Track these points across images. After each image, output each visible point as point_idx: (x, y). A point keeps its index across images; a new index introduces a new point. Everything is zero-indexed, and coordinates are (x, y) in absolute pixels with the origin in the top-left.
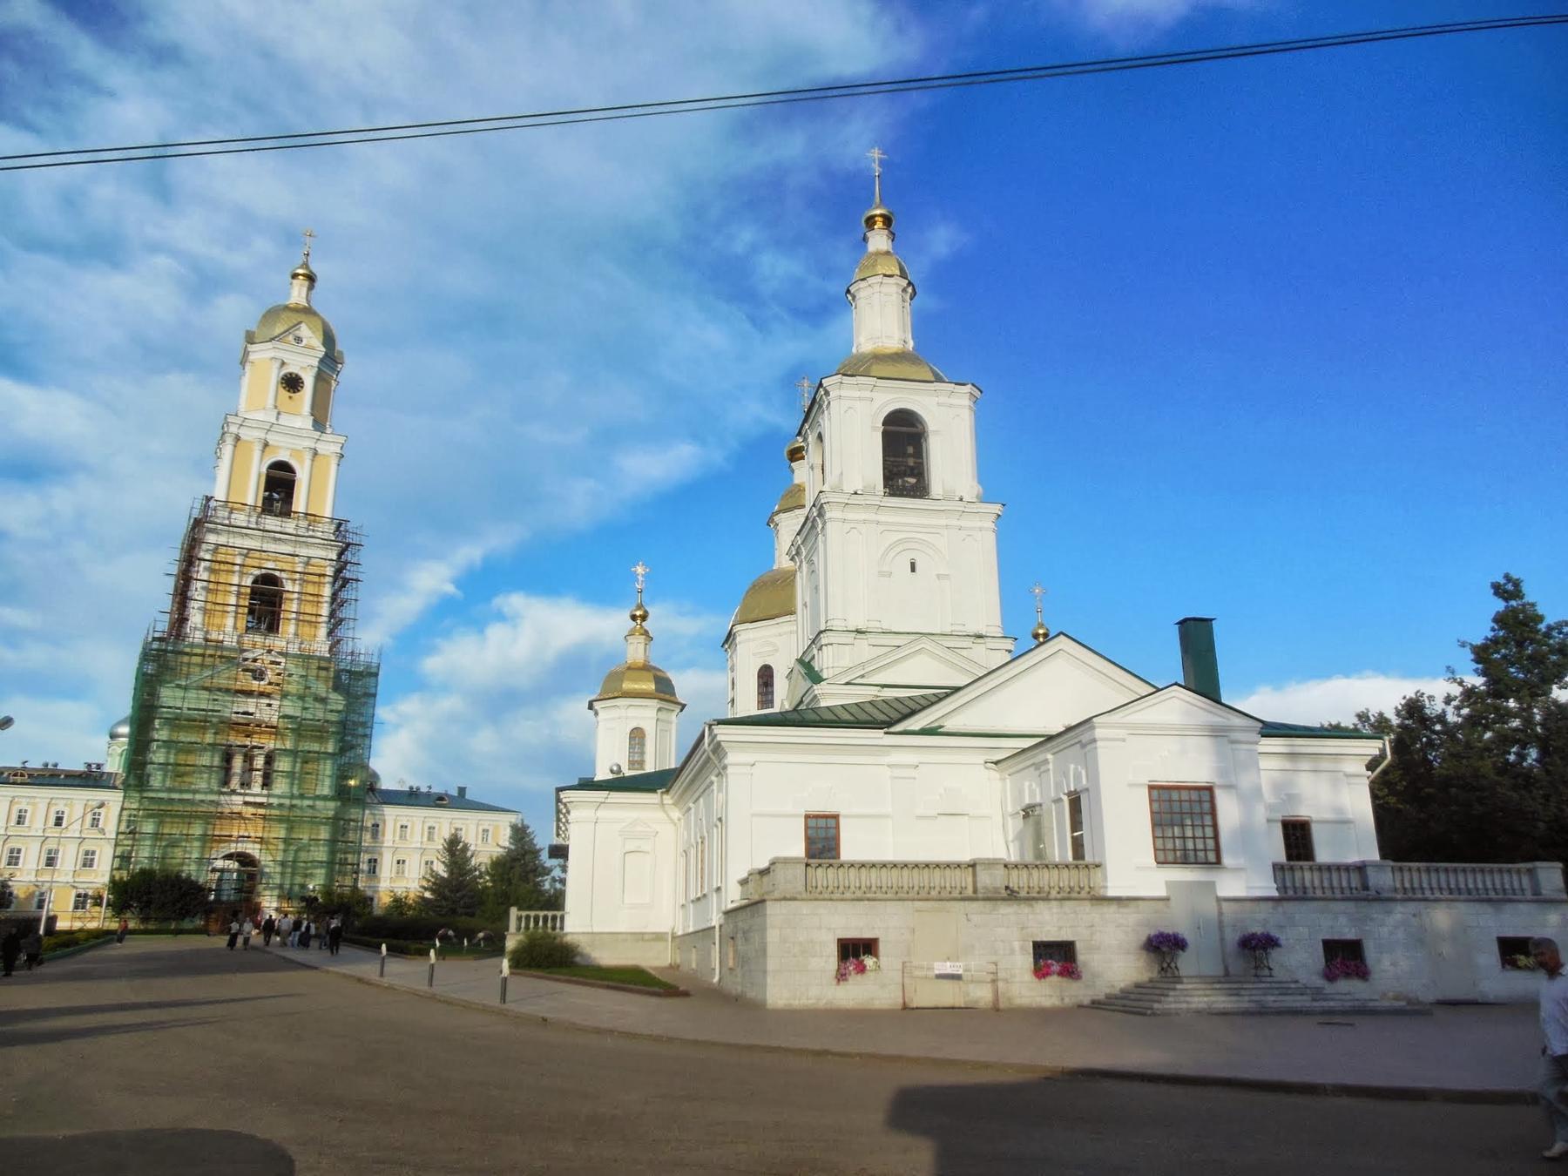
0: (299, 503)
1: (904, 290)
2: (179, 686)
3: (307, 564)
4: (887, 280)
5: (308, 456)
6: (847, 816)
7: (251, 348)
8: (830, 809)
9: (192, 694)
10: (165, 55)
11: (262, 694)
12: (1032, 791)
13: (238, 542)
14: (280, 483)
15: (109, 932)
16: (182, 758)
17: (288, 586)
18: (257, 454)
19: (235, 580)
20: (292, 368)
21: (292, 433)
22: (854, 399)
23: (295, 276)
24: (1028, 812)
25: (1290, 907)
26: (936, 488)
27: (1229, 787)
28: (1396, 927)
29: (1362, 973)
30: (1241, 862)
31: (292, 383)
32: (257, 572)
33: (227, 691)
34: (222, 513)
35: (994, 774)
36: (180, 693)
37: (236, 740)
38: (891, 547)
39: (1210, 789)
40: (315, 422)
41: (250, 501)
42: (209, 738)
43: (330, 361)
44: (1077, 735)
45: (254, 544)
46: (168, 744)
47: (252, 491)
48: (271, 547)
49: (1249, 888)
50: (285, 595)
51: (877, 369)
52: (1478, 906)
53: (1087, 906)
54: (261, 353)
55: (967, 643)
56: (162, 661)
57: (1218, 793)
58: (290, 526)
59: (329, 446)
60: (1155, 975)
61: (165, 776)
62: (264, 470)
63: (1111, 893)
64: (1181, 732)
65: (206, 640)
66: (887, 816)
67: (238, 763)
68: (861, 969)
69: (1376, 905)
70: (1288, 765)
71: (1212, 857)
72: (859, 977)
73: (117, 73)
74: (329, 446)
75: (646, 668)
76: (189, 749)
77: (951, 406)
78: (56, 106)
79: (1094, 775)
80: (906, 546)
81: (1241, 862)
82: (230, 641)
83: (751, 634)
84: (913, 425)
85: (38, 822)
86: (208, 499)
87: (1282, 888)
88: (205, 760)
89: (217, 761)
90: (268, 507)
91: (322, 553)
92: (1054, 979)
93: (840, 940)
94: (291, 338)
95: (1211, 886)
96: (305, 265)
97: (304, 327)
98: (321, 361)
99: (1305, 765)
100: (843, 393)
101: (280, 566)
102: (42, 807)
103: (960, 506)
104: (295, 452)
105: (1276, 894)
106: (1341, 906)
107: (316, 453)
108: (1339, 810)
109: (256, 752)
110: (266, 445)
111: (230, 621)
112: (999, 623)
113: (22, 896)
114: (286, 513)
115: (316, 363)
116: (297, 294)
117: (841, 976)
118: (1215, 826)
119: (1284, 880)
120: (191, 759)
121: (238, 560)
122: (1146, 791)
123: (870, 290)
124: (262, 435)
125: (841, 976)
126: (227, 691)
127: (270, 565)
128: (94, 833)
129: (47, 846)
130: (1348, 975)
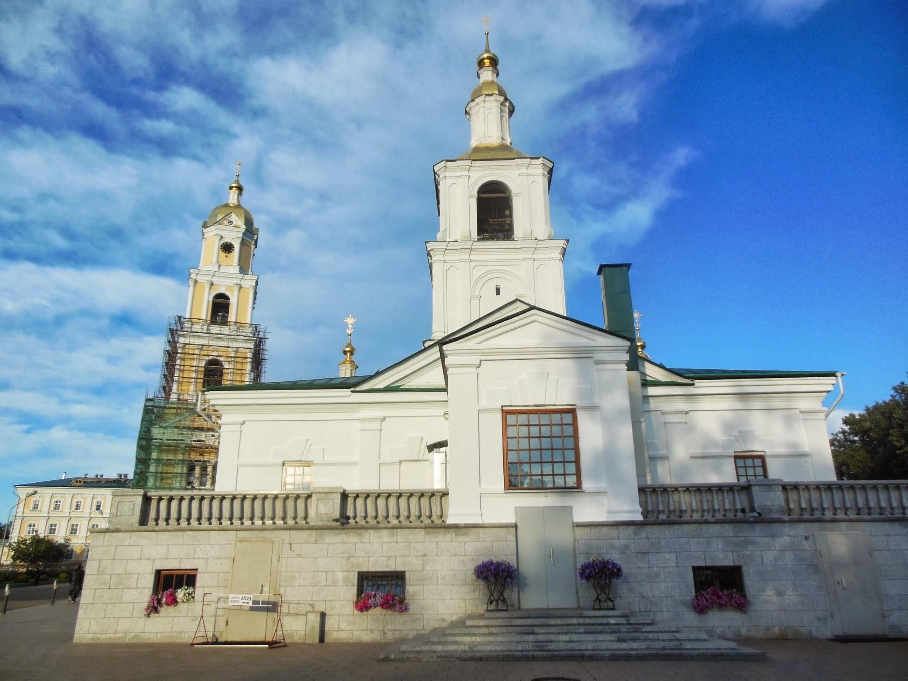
0: (232, 317)
1: (502, 104)
2: (161, 427)
3: (236, 352)
4: (488, 98)
7: (205, 230)
9: (169, 431)
10: (258, 113)
11: (209, 430)
13: (197, 341)
14: (220, 306)
16: (166, 469)
17: (226, 365)
18: (207, 289)
19: (195, 363)
20: (227, 239)
21: (226, 276)
23: (231, 188)
25: (655, 532)
27: (592, 408)
28: (783, 551)
29: (741, 604)
30: (603, 485)
33: (189, 428)
34: (187, 325)
36: (162, 430)
37: (194, 456)
39: (572, 411)
40: (241, 269)
41: (204, 317)
42: (180, 456)
43: (250, 231)
45: (205, 341)
46: (158, 461)
47: (204, 311)
48: (216, 343)
49: (610, 512)
50: (225, 371)
52: (887, 526)
53: (420, 535)
54: (211, 232)
56: (153, 414)
57: (580, 414)
58: (225, 330)
59: (248, 282)
60: (481, 609)
61: (156, 480)
62: (211, 299)
63: (450, 521)
64: (538, 354)
65: (179, 399)
66: (355, 463)
67: (197, 470)
68: (173, 601)
69: (758, 528)
70: (737, 405)
71: (571, 481)
72: (171, 609)
73: (237, 126)
74: (248, 282)
76: (169, 463)
78: (209, 145)
80: (490, 277)
81: (603, 485)
82: (191, 399)
84: (504, 192)
86: (180, 318)
87: (645, 513)
88: (178, 469)
89: (185, 470)
90: (214, 321)
91: (244, 345)
92: (378, 611)
93: (158, 572)
94: (226, 222)
95: (567, 510)
96: (237, 181)
97: (233, 215)
98: (244, 234)
99: (757, 404)
100: (448, 174)
101: (222, 354)
104: (228, 287)
105: (640, 517)
106: (714, 529)
107: (240, 287)
108: (794, 445)
109: (208, 464)
110: (212, 284)
111: (192, 388)
113: (78, 552)
114: (225, 323)
115: (240, 235)
116: (232, 198)
117: (153, 609)
118: (576, 450)
119: (646, 502)
120: (170, 469)
121: (197, 352)
122: (733, 459)
123: (477, 108)
124: (209, 279)
125: (153, 609)
126: (189, 428)
127: (215, 353)
128: (98, 514)
129: (50, 522)
130: (722, 607)
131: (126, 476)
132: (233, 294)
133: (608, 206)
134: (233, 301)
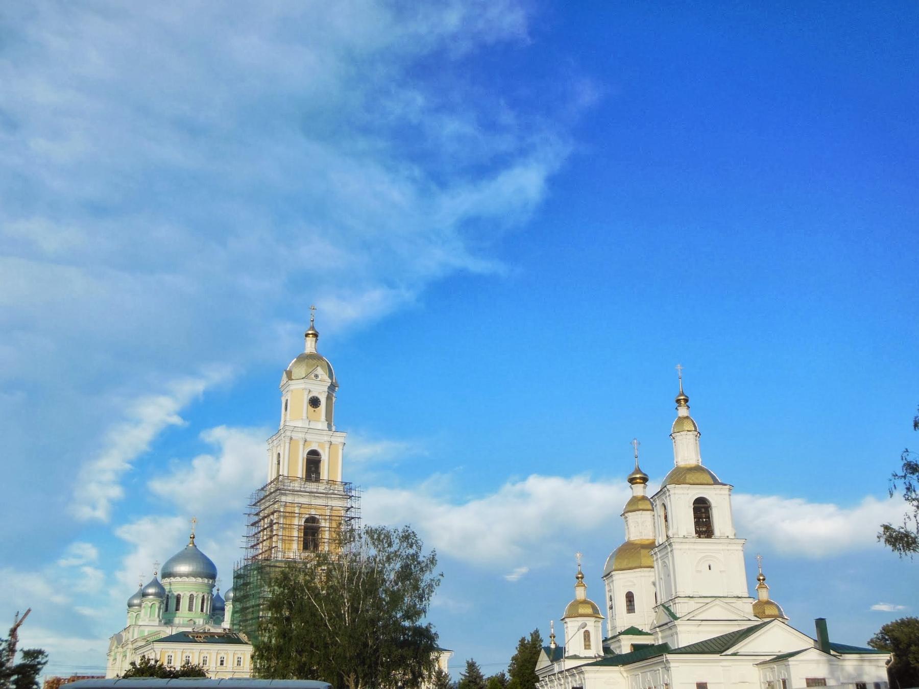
0: (324, 475)
3: (331, 509)
5: (327, 446)
8: (704, 681)
12: (770, 677)
14: (313, 462)
17: (323, 524)
18: (301, 446)
23: (307, 335)
24: (769, 683)
31: (314, 402)
32: (307, 516)
35: (756, 668)
38: (700, 560)
44: (782, 658)
47: (300, 470)
51: (690, 477)
55: (734, 600)
58: (322, 488)
62: (305, 456)
75: (585, 602)
79: (789, 675)
83: (621, 576)
94: (313, 376)
96: (313, 328)
97: (319, 368)
98: (329, 388)
102: (179, 654)
103: (728, 541)
104: (321, 444)
112: (746, 590)
114: (318, 480)
115: (326, 389)
131: (542, 641)
132: (323, 449)
133: (484, 169)
134: (324, 457)
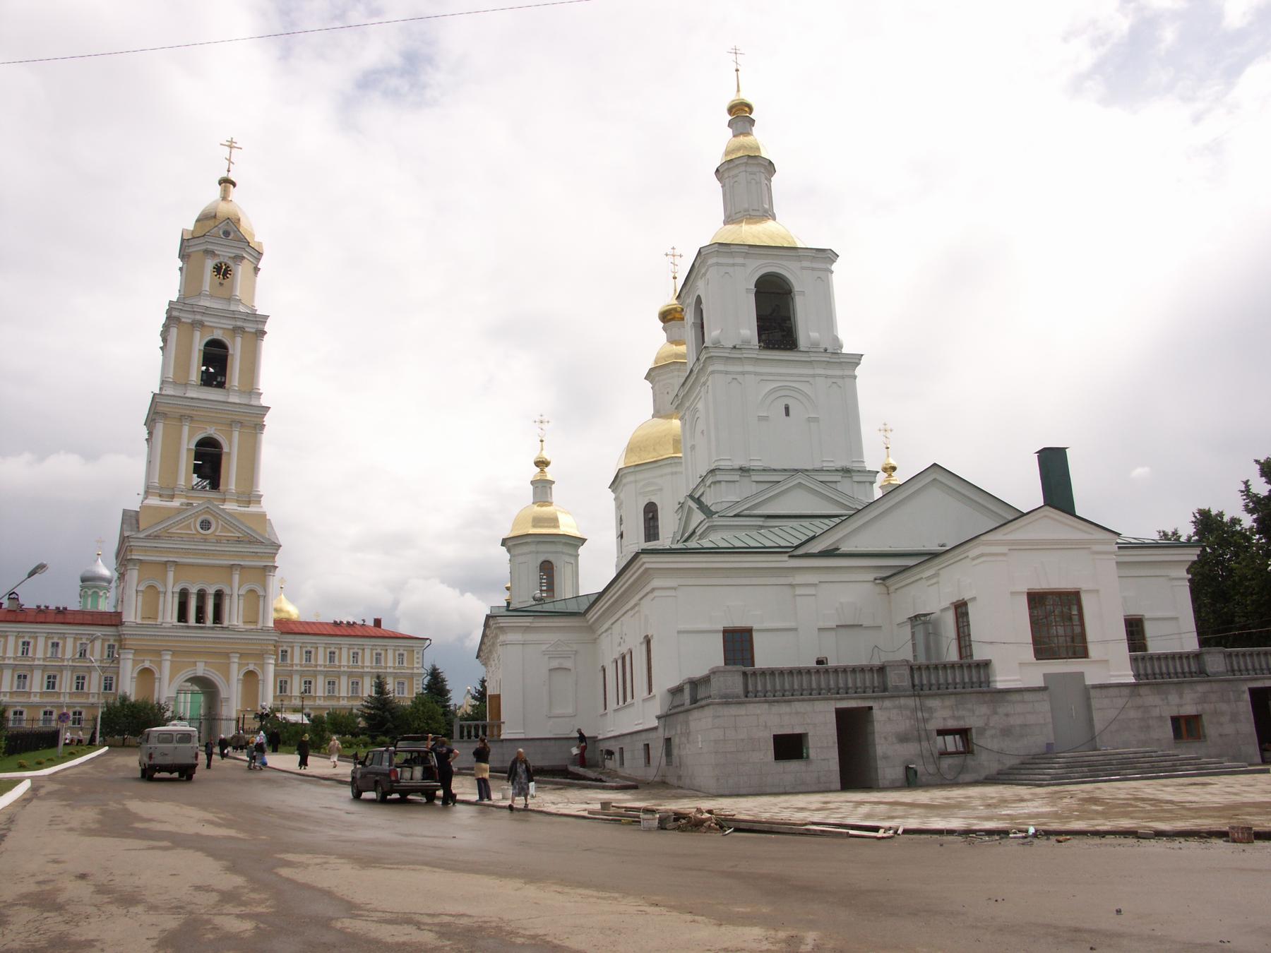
6: (1086, 591)
15: (235, 748)
22: (728, 265)
26: (802, 342)
77: (813, 269)
80: (783, 393)
85: (69, 649)
105: (1133, 680)
